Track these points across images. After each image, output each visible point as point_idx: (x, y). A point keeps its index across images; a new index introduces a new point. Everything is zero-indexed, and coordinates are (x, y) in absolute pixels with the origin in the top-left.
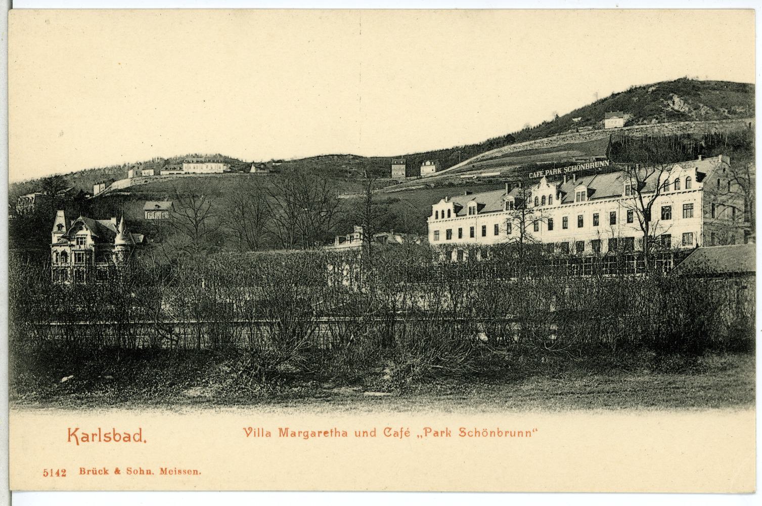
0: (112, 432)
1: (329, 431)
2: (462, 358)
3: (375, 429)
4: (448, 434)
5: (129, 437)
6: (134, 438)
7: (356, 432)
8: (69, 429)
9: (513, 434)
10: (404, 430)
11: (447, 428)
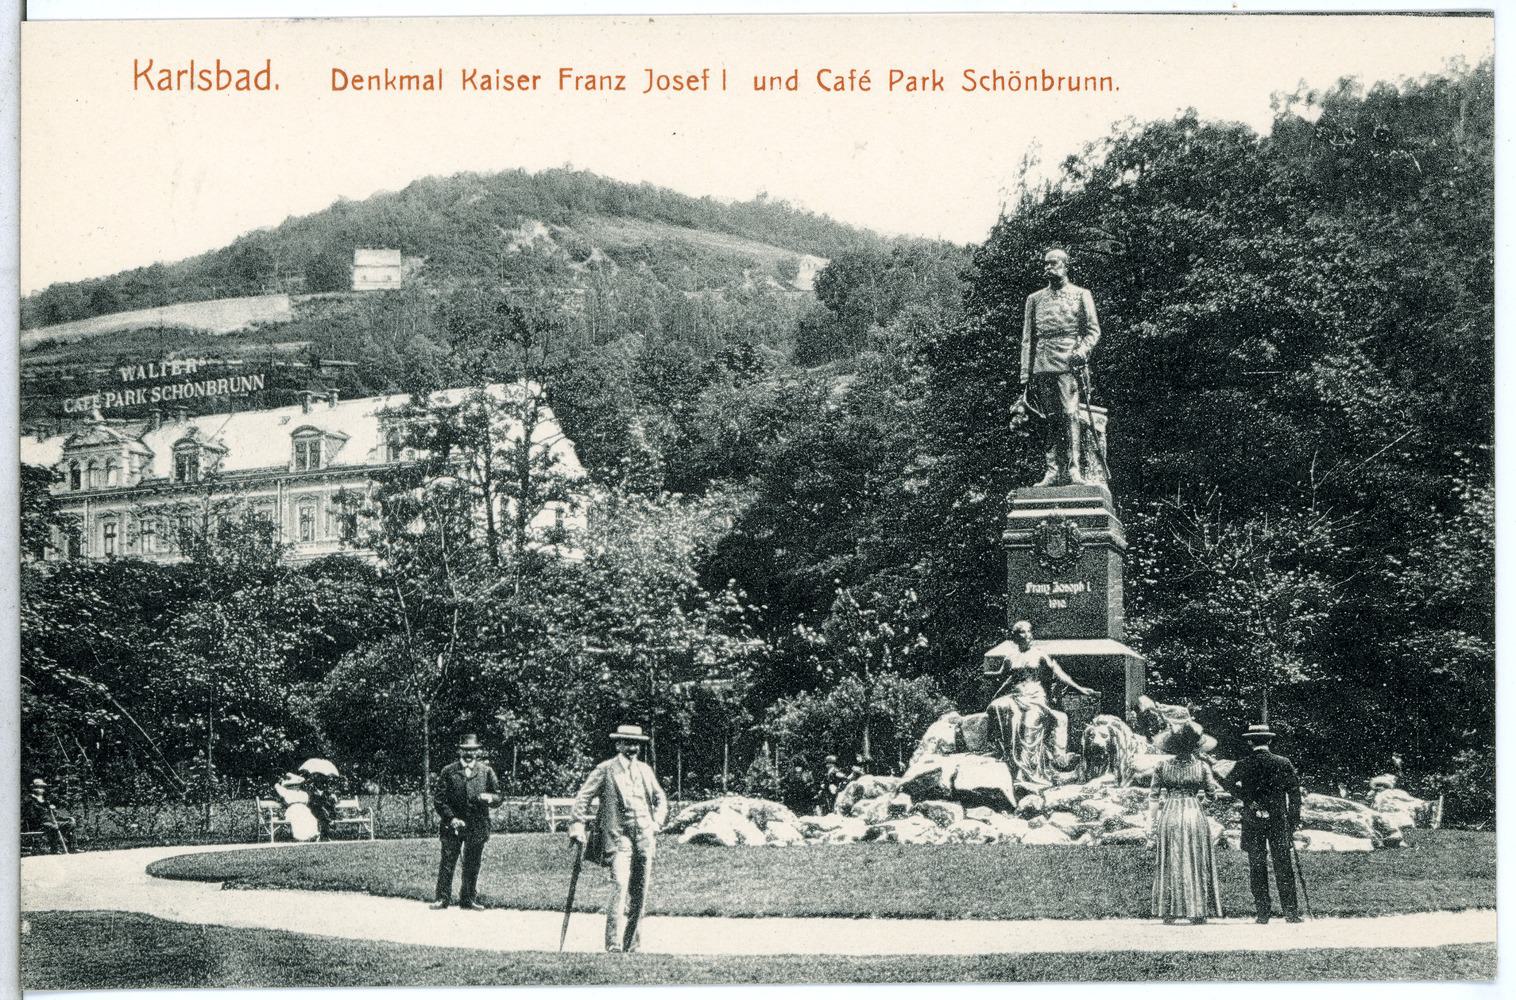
0: (214, 69)
1: (699, 75)
2: (116, 711)
7: (756, 78)
8: (464, 71)
9: (1074, 85)
10: (858, 75)
11: (387, 70)
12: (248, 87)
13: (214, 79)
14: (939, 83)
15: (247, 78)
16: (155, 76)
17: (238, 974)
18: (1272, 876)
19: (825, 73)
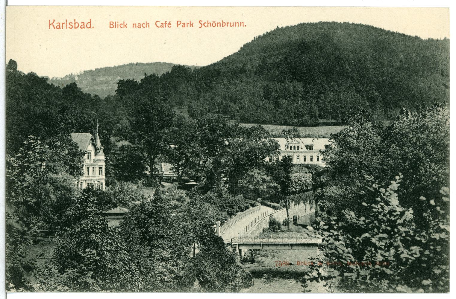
0: (73, 22)
3: (90, 20)
4: (192, 25)
5: (140, 25)
6: (87, 25)
9: (232, 25)
10: (168, 23)
12: (84, 28)
13: (74, 25)
14: (125, 26)
15: (84, 25)
16: (55, 25)
17: (448, 279)
18: (367, 187)
19: (158, 22)
